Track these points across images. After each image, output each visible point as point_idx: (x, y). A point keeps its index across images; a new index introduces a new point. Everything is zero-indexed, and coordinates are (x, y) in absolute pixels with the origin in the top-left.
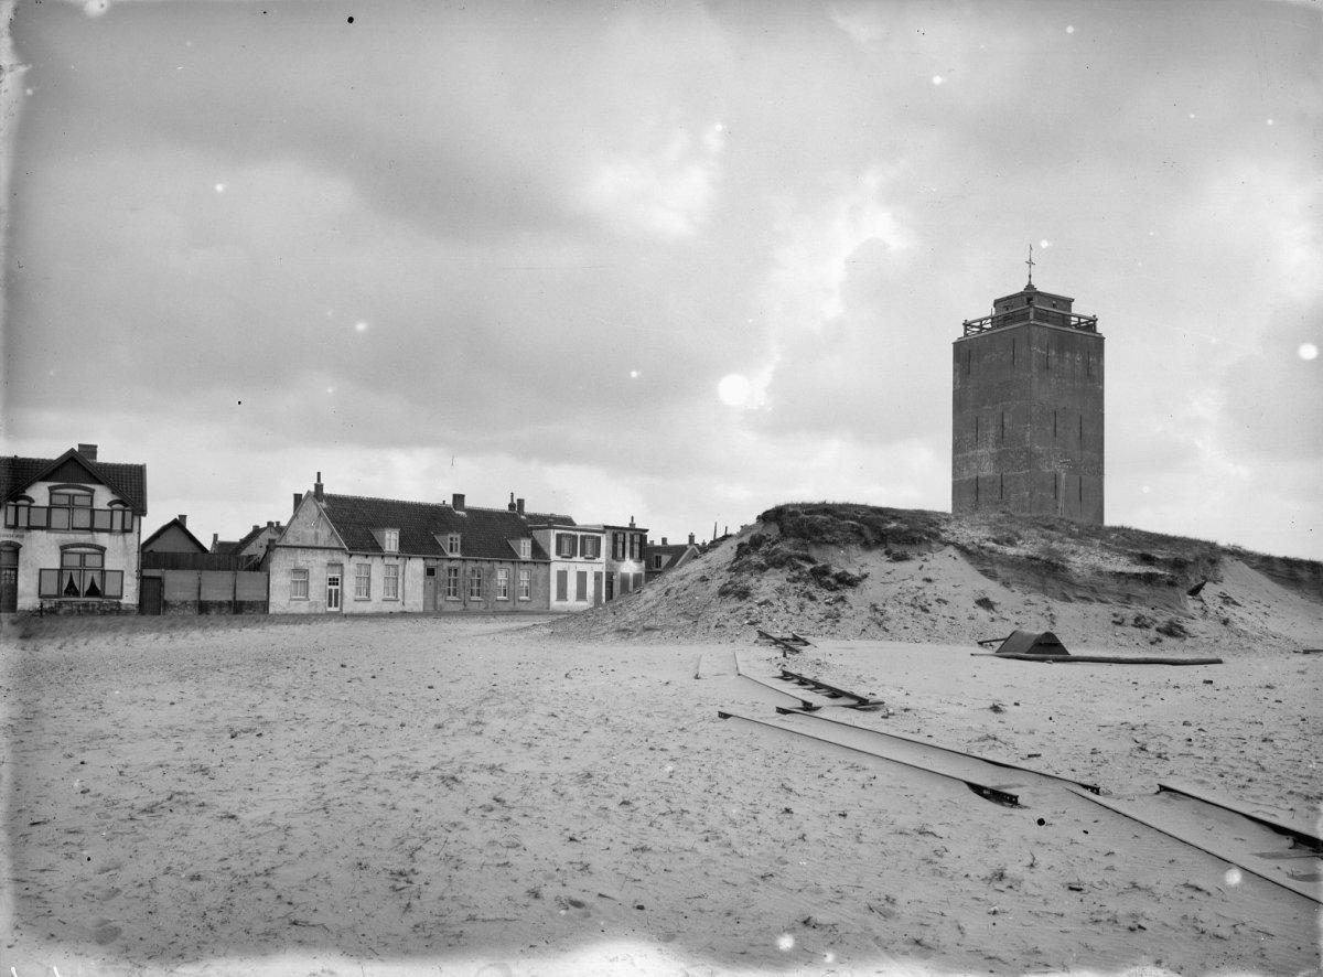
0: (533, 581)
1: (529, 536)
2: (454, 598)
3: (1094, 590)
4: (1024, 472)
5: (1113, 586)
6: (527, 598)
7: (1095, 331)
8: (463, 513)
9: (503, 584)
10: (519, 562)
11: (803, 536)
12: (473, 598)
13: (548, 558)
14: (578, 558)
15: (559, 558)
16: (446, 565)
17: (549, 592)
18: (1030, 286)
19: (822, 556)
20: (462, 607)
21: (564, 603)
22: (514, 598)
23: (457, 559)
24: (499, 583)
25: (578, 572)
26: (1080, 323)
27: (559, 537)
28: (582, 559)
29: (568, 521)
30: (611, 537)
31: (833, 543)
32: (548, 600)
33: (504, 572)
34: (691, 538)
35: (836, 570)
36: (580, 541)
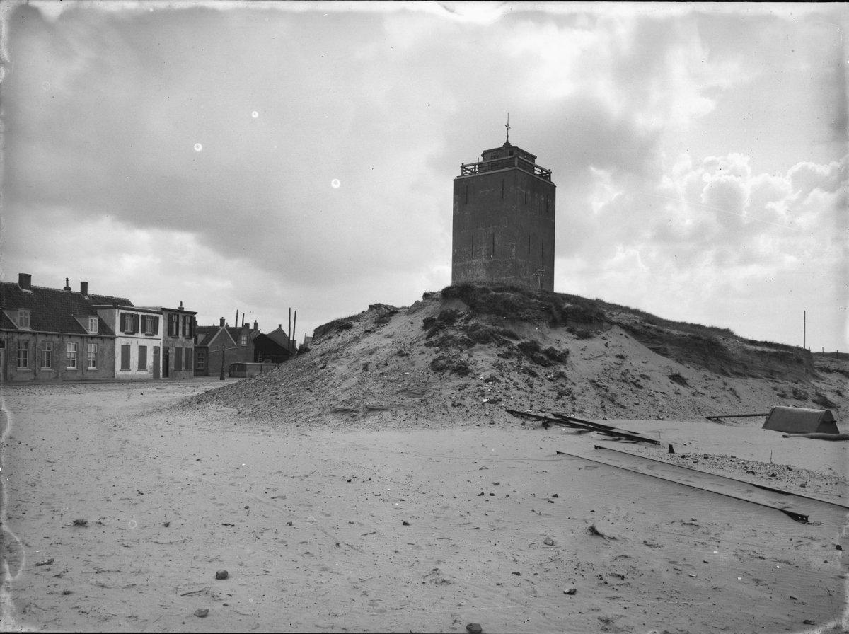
0: (100, 354)
1: (95, 314)
2: (25, 369)
3: (745, 367)
4: (510, 277)
5: (760, 364)
6: (25, 369)
7: (550, 180)
8: (30, 292)
9: (72, 356)
10: (87, 337)
11: (498, 313)
12: (44, 369)
13: (113, 333)
14: (140, 335)
15: (123, 334)
16: (16, 337)
17: (114, 363)
18: (507, 144)
19: (531, 333)
20: (33, 377)
21: (127, 373)
22: (82, 368)
23: (27, 333)
24: (68, 356)
25: (140, 346)
26: (542, 174)
27: (122, 315)
28: (143, 336)
29: (126, 303)
30: (167, 318)
31: (527, 320)
32: (114, 370)
33: (73, 346)
34: (222, 321)
35: (546, 346)
36: (141, 321)
